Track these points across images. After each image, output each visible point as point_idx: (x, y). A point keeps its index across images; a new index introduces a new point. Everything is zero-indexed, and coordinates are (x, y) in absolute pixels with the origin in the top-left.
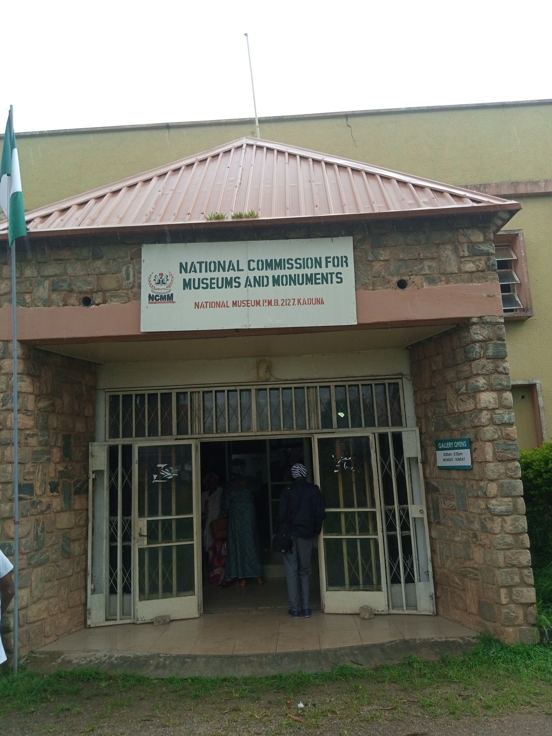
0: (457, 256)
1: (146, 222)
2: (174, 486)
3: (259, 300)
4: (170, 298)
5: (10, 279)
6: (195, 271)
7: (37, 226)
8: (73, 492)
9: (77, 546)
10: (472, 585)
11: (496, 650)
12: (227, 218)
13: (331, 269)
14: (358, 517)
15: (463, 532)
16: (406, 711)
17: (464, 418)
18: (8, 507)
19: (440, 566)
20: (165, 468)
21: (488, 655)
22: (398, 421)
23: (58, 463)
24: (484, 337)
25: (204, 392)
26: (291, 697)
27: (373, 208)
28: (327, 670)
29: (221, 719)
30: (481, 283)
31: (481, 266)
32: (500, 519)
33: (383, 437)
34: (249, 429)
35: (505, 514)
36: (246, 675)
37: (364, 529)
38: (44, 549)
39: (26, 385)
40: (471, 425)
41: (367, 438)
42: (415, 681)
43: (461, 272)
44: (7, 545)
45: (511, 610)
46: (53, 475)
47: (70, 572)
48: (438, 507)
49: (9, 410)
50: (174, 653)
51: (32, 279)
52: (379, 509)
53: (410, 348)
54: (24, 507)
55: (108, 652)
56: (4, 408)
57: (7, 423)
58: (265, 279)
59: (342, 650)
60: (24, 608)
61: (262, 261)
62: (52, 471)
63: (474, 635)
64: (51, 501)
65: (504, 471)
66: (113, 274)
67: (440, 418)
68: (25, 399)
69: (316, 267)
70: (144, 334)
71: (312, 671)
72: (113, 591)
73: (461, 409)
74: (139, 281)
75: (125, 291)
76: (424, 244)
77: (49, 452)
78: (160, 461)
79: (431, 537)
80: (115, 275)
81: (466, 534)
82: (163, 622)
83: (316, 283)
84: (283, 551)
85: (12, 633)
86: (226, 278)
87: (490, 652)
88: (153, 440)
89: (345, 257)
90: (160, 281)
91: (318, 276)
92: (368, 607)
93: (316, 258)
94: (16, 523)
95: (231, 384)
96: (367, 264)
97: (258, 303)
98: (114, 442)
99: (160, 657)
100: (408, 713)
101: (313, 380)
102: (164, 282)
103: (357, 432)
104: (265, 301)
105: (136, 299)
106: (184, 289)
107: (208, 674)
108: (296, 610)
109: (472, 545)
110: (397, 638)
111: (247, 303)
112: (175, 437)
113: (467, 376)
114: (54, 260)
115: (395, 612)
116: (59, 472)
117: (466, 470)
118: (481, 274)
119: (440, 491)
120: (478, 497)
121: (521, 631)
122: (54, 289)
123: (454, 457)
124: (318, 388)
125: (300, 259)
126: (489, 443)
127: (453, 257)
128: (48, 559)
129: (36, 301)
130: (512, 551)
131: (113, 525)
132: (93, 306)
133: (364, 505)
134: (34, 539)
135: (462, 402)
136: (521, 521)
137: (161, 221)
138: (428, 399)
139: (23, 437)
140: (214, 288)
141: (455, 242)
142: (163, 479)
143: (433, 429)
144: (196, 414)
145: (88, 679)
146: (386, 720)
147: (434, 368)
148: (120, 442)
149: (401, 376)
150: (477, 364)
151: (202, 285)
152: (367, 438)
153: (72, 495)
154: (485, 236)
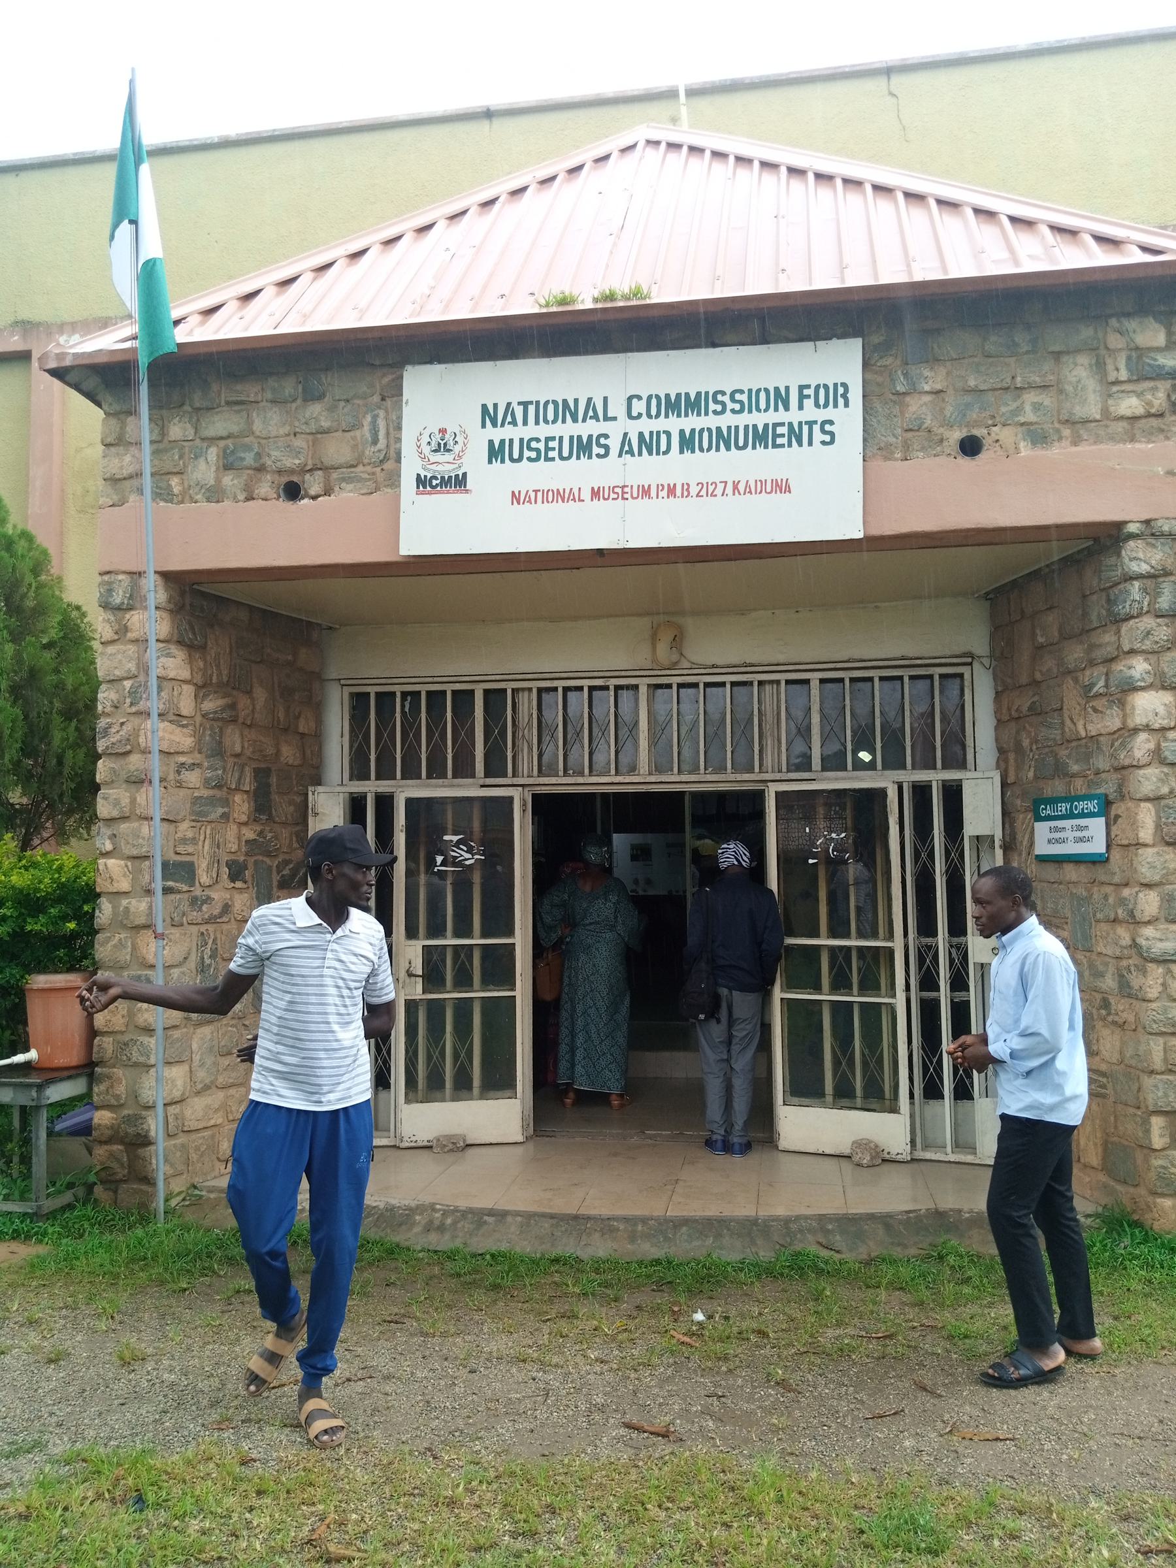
0: (1101, 381)
2: (477, 878)
4: (460, 482)
5: (138, 444)
6: (514, 423)
8: (275, 883)
11: (1132, 1240)
12: (583, 301)
13: (811, 412)
14: (859, 958)
17: (1098, 748)
20: (459, 842)
21: (1113, 1250)
22: (957, 757)
23: (246, 824)
26: (682, 1300)
27: (910, 273)
28: (765, 1254)
29: (536, 1330)
30: (1153, 442)
31: (1156, 403)
32: (1160, 970)
33: (921, 792)
34: (633, 769)
36: (601, 1253)
39: (176, 664)
41: (882, 793)
43: (1108, 419)
44: (143, 978)
50: (463, 1204)
51: (185, 444)
53: (991, 596)
56: (134, 709)
58: (663, 438)
61: (658, 397)
62: (233, 838)
64: (231, 899)
67: (1047, 750)
68: (175, 693)
69: (776, 409)
70: (412, 560)
71: (734, 1257)
73: (1093, 730)
75: (369, 468)
76: (1027, 352)
77: (226, 802)
78: (450, 831)
80: (348, 435)
82: (451, 1146)
83: (775, 446)
84: (702, 1017)
85: (152, 1148)
86: (580, 437)
88: (437, 786)
89: (844, 385)
91: (780, 430)
92: (871, 1142)
93: (777, 389)
96: (892, 401)
97: (645, 492)
98: (358, 787)
99: (434, 1210)
100: (916, 1347)
101: (775, 667)
102: (448, 447)
104: (660, 488)
106: (490, 462)
107: (525, 1247)
108: (719, 1137)
110: (924, 1205)
111: (621, 493)
112: (481, 782)
113: (1109, 656)
114: (228, 403)
115: (929, 1155)
117: (1094, 863)
118: (1154, 422)
122: (227, 466)
123: (1070, 835)
124: (783, 683)
125: (741, 392)
126: (1148, 805)
127: (1091, 384)
129: (191, 492)
132: (306, 501)
133: (875, 935)
135: (1095, 715)
138: (1025, 709)
139: (173, 767)
140: (553, 459)
141: (1097, 348)
142: (454, 864)
143: (1031, 774)
144: (523, 736)
145: (295, 1242)
147: (1041, 640)
148: (371, 787)
149: (969, 658)
150: (1131, 629)
151: (527, 453)
153: (275, 889)
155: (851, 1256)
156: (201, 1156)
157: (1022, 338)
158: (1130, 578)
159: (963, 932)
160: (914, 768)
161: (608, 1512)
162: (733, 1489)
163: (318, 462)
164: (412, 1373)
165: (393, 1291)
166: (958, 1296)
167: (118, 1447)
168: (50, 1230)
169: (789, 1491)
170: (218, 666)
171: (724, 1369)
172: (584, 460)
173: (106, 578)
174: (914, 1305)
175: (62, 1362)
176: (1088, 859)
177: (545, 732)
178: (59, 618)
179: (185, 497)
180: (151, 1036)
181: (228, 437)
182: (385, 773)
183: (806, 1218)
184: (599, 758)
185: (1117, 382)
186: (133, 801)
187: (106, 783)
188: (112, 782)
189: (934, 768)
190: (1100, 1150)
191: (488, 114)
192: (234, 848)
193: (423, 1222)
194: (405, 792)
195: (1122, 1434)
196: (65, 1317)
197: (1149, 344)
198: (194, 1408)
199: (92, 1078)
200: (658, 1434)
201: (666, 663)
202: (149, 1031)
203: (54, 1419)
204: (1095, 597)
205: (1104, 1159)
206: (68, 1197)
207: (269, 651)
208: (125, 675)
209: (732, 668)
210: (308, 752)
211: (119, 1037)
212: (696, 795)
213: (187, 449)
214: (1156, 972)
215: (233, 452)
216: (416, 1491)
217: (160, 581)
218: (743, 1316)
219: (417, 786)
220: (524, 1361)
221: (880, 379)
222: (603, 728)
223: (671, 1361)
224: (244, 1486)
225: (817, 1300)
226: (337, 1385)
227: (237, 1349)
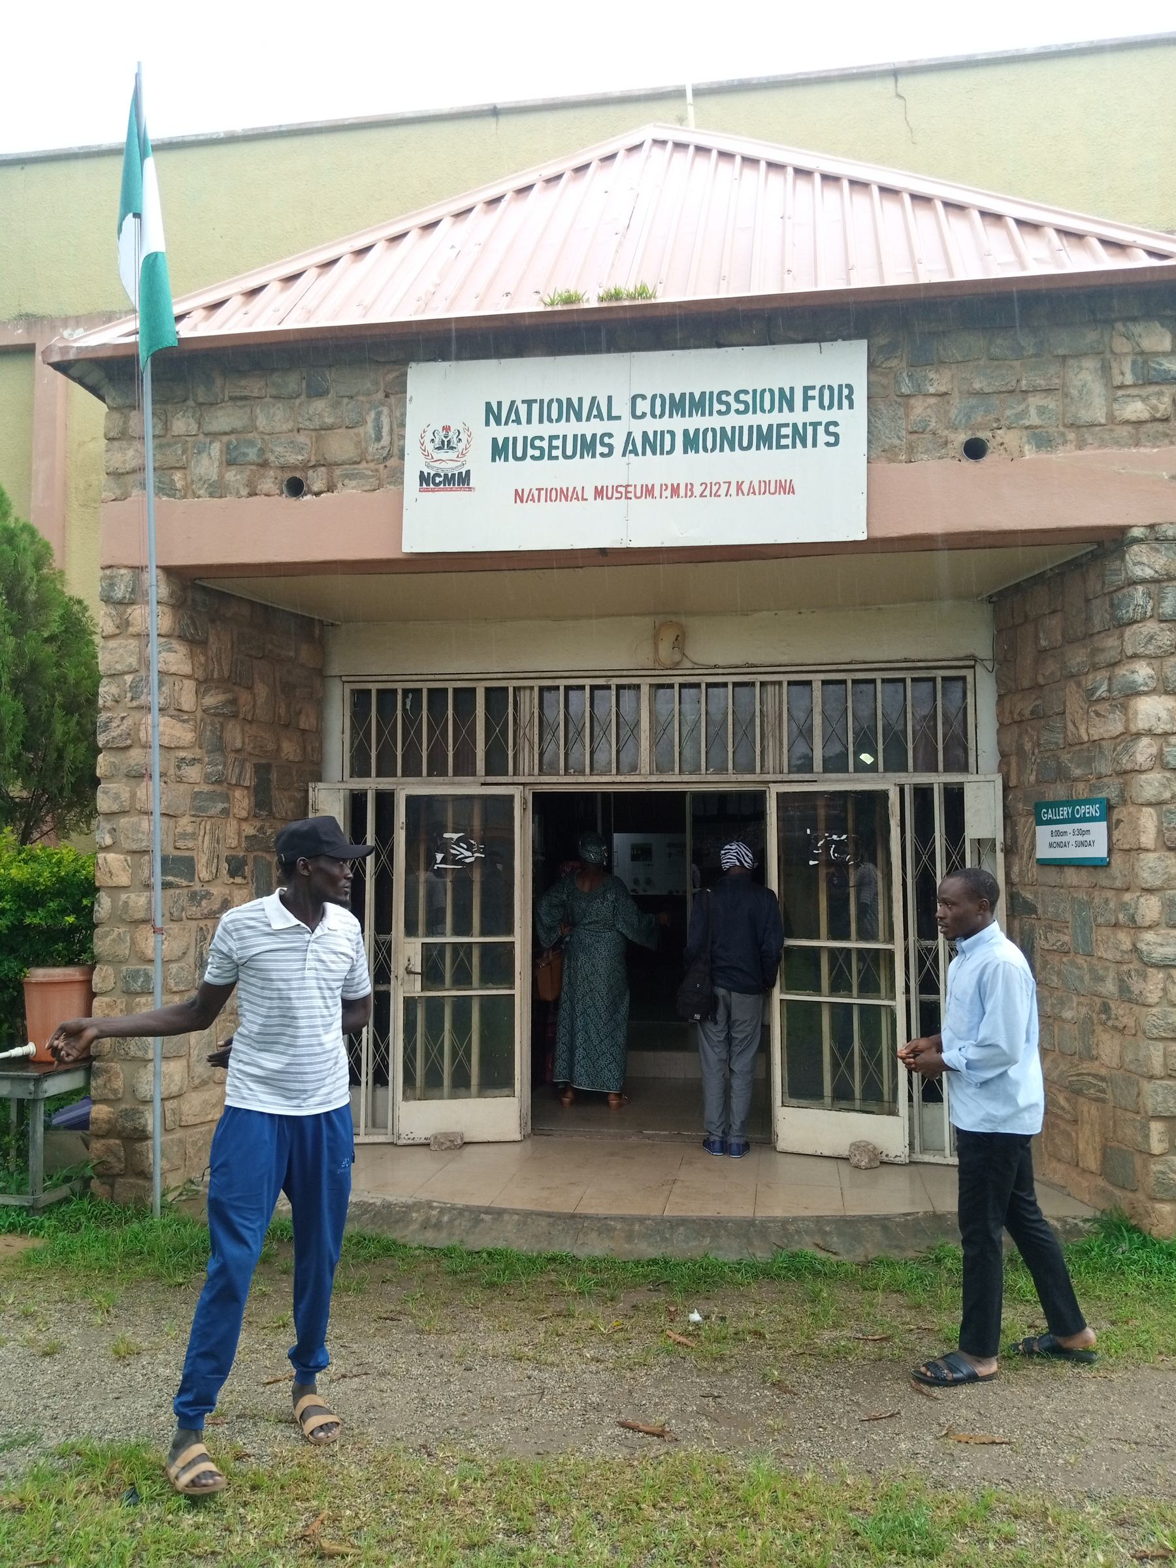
0: (1106, 385)
2: (477, 876)
3: (653, 486)
4: (462, 480)
5: (142, 438)
6: (518, 421)
7: (196, 326)
10: (1094, 1111)
11: (1131, 1246)
12: (588, 300)
13: (815, 413)
15: (1082, 999)
16: (910, 1346)
17: (1100, 752)
18: (142, 900)
20: (459, 840)
22: (959, 760)
23: (245, 820)
24: (1156, 572)
25: (542, 689)
28: (762, 1255)
30: (1158, 447)
31: (1162, 407)
32: (1161, 975)
33: (923, 795)
34: (634, 769)
39: (177, 659)
40: (1114, 770)
41: (884, 795)
42: (942, 1293)
43: (1113, 423)
45: (1170, 1167)
46: (234, 843)
48: (1033, 947)
50: (460, 1202)
51: (188, 439)
53: (994, 599)
56: (135, 704)
58: (668, 437)
59: (799, 1223)
60: (174, 1097)
61: (662, 396)
62: (233, 834)
63: (1088, 1213)
64: (230, 894)
66: (347, 427)
67: (1049, 753)
68: (177, 688)
69: (781, 410)
71: (733, 1258)
73: (1096, 734)
74: (401, 443)
75: (372, 465)
76: (1035, 355)
77: (226, 798)
81: (1087, 1005)
82: (448, 1144)
83: (779, 447)
84: (697, 1017)
85: (150, 1142)
86: (583, 436)
87: (1116, 1250)
89: (849, 387)
90: (443, 442)
91: (784, 431)
92: (869, 1144)
93: (781, 390)
94: (156, 931)
95: (597, 673)
97: (649, 491)
98: (359, 784)
99: (431, 1208)
102: (451, 445)
104: (664, 487)
106: (494, 460)
107: (522, 1245)
108: (717, 1138)
109: (1099, 1029)
110: (922, 1208)
111: (624, 492)
112: (482, 780)
113: (1113, 661)
114: (232, 399)
115: (927, 1158)
116: (246, 837)
117: (1095, 867)
118: (1160, 427)
119: (1039, 912)
120: (1116, 925)
123: (1071, 839)
124: (785, 685)
125: (746, 392)
126: (1150, 810)
127: (1097, 388)
129: (194, 486)
132: (309, 497)
133: (873, 937)
134: (196, 966)
135: (1097, 719)
138: (1027, 713)
139: (173, 762)
140: (557, 458)
143: (1033, 778)
144: (524, 734)
146: (864, 1358)
147: (1044, 643)
148: (371, 784)
149: (972, 661)
150: (1134, 633)
151: (530, 452)
152: (884, 795)
157: (1028, 343)
158: (1133, 583)
159: (388, 930)
160: (915, 770)
162: (727, 1489)
163: (320, 458)
164: (407, 1370)
165: (388, 1288)
167: (112, 1440)
168: (47, 1224)
169: (784, 1493)
170: (219, 661)
171: (720, 1369)
172: (588, 458)
173: (108, 572)
174: (910, 1308)
175: (57, 1356)
176: (1088, 863)
177: (547, 730)
178: (61, 612)
179: (188, 492)
181: (232, 432)
182: (386, 770)
183: (804, 1219)
184: (600, 757)
186: (133, 795)
187: (106, 778)
189: (936, 771)
190: (1099, 1154)
191: (495, 112)
192: (234, 843)
193: (420, 1219)
194: (405, 789)
195: (1118, 1439)
196: (61, 1310)
199: (89, 1072)
200: (654, 1434)
201: (668, 663)
203: (48, 1413)
204: (1098, 602)
205: (1102, 1164)
206: (64, 1191)
207: (270, 647)
208: (126, 669)
210: (309, 748)
213: (190, 445)
215: (235, 447)
216: (411, 1488)
218: (739, 1318)
219: (417, 784)
220: (520, 1359)
221: (884, 381)
222: (605, 727)
223: (667, 1360)
226: (332, 1381)
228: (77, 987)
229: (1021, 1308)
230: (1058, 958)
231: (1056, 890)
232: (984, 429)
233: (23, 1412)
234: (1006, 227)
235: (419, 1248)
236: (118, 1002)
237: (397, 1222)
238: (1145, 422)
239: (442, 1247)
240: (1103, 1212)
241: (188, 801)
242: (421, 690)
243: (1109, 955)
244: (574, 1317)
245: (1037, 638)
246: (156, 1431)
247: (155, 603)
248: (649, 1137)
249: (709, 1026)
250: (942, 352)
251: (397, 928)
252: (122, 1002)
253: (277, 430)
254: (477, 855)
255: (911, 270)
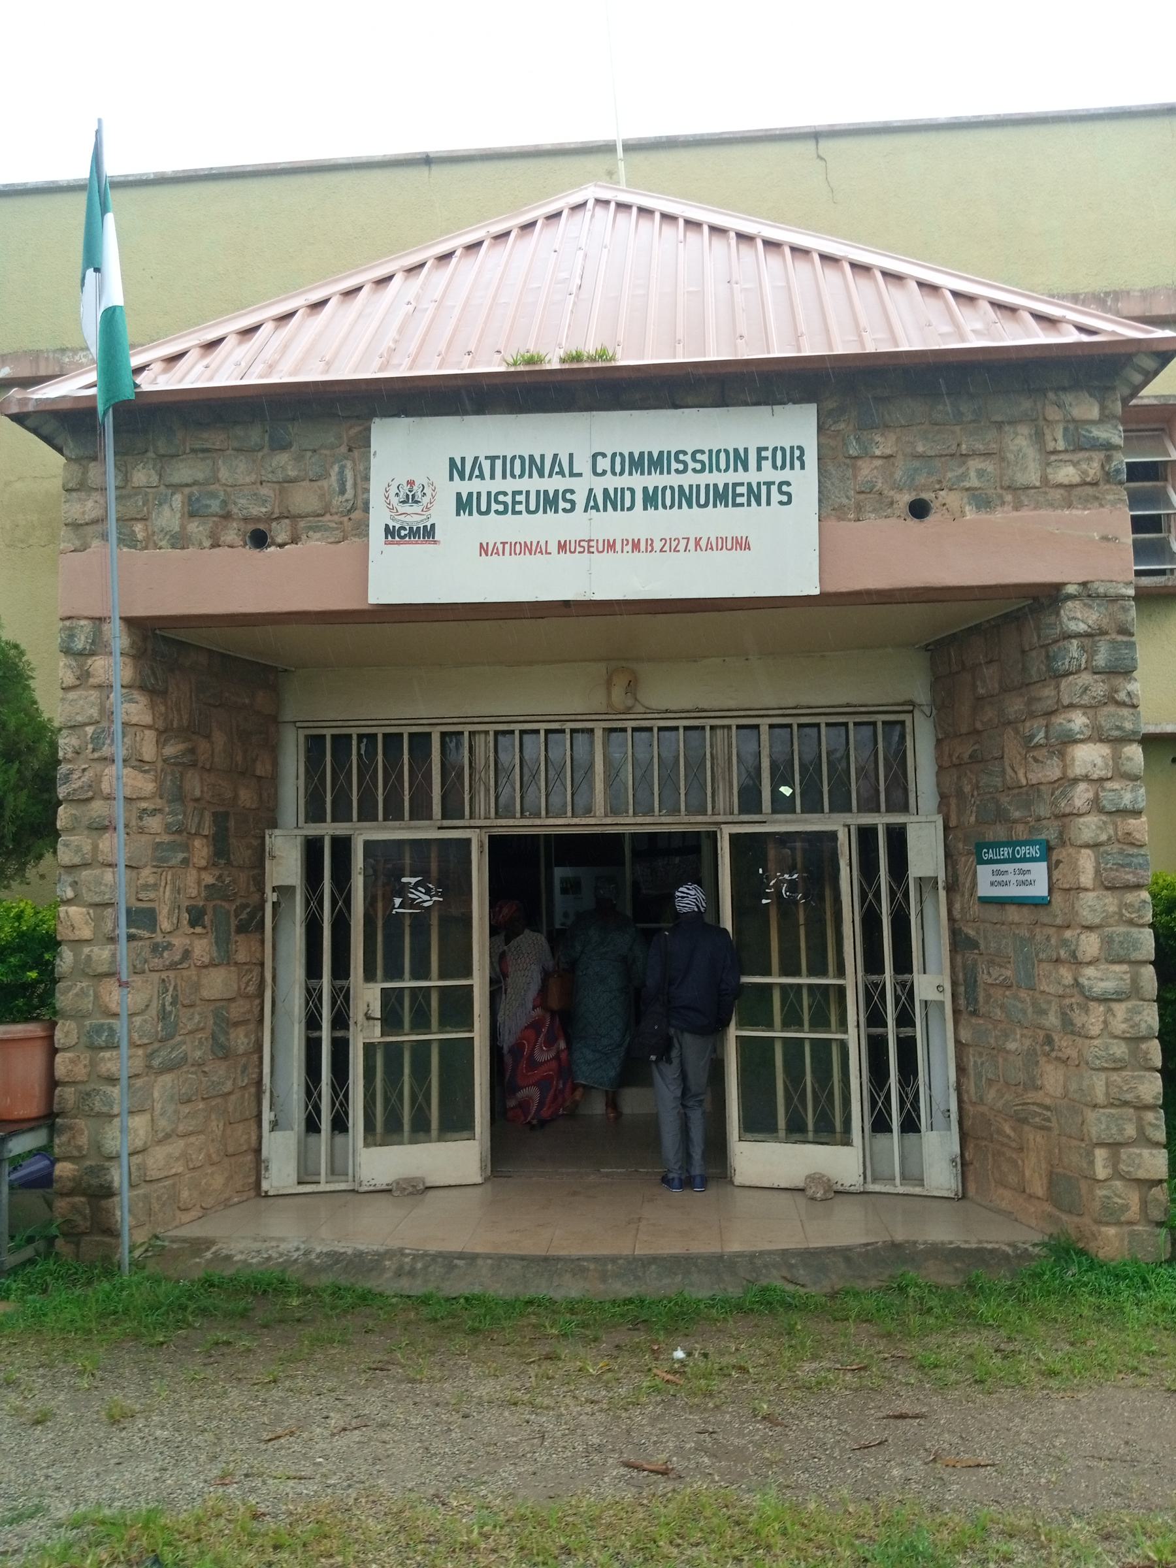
0: (1040, 450)
1: (381, 370)
4: (427, 533)
5: (103, 489)
6: (481, 476)
7: (155, 378)
8: (233, 928)
9: (242, 1036)
10: (1039, 1139)
11: (1080, 1268)
12: (549, 361)
13: (768, 473)
15: (1025, 1031)
16: (887, 1374)
19: (974, 1099)
20: (417, 884)
22: (901, 802)
23: (205, 868)
25: (497, 733)
27: (862, 343)
28: (734, 1292)
31: (1091, 472)
32: (1102, 1008)
33: (867, 835)
34: (589, 811)
35: (1114, 997)
36: (574, 1294)
37: (820, 1021)
38: (178, 1039)
39: (137, 710)
41: (833, 836)
43: (1046, 485)
46: (194, 893)
47: (228, 1086)
48: (976, 981)
49: (105, 759)
50: (433, 1248)
52: (852, 981)
54: (138, 955)
55: (303, 1242)
56: (96, 755)
57: (103, 787)
58: (628, 494)
62: (193, 883)
63: (1037, 1238)
65: (1116, 909)
66: (311, 480)
69: (736, 470)
71: (704, 1294)
72: (312, 1126)
73: (1034, 778)
75: (336, 518)
77: (186, 847)
78: (407, 872)
79: (957, 1042)
82: (411, 1189)
83: (735, 505)
84: (653, 1058)
85: (116, 1199)
86: (546, 492)
89: (800, 448)
90: (407, 496)
91: (739, 490)
93: (736, 451)
97: (611, 546)
98: (314, 830)
101: (726, 712)
103: (812, 823)
105: (358, 535)
106: (458, 514)
107: (498, 1289)
109: (1042, 1060)
110: (880, 1238)
111: (587, 546)
112: (439, 824)
113: (1049, 709)
114: (193, 451)
115: (877, 1188)
117: (1036, 905)
118: (1090, 490)
119: (982, 947)
120: (1058, 960)
121: (1132, 1234)
123: (1013, 878)
124: (734, 728)
125: (703, 452)
126: (1088, 851)
127: (1031, 452)
128: (185, 1059)
130: (1124, 1073)
131: (312, 996)
132: (272, 549)
133: (824, 973)
136: (1145, 1013)
137: (411, 368)
138: (966, 756)
139: (135, 813)
140: (520, 513)
143: (973, 819)
145: (265, 1291)
147: (981, 691)
148: (328, 830)
149: (911, 706)
151: (494, 506)
152: (833, 836)
154: (1103, 408)
155: (816, 1290)
156: (164, 1205)
158: (1069, 636)
159: (347, 976)
160: (859, 811)
161: (622, 1551)
162: (738, 1523)
164: (407, 1421)
165: (373, 1338)
166: (923, 1326)
167: (122, 1507)
168: (14, 1286)
169: (793, 1524)
170: (179, 710)
171: (711, 1405)
173: (67, 623)
174: (882, 1336)
175: (49, 1424)
176: (1029, 901)
177: (502, 775)
179: (148, 543)
180: (114, 1086)
182: (339, 814)
183: (770, 1253)
184: (555, 799)
185: (1055, 452)
188: (74, 828)
189: (878, 811)
190: (1045, 1181)
191: (427, 161)
192: (194, 893)
193: (394, 1267)
194: (362, 834)
195: (1093, 1457)
196: (43, 1376)
197: (1085, 417)
198: (193, 1464)
199: (52, 1130)
200: (657, 1472)
202: (112, 1080)
203: (51, 1483)
204: (1034, 654)
205: (1049, 1188)
206: (28, 1252)
207: (227, 694)
209: (684, 713)
210: (265, 795)
211: (80, 1087)
212: (634, 835)
213: (150, 497)
214: (1099, 1009)
215: (198, 499)
216: (432, 1539)
217: (122, 624)
218: (722, 1354)
220: (515, 1404)
221: (833, 443)
223: (659, 1399)
224: (258, 1542)
225: (789, 1334)
226: (333, 1435)
227: (226, 1402)
228: (39, 1042)
229: (985, 1333)
230: (1001, 992)
231: (998, 926)
232: (928, 490)
233: (24, 1484)
234: (943, 297)
235: (395, 1296)
236: (82, 1057)
237: (371, 1270)
238: (1077, 485)
239: (419, 1294)
240: (1051, 1236)
241: (150, 852)
242: (376, 735)
243: (1051, 989)
244: (560, 1359)
245: (974, 687)
246: (165, 1494)
247: (118, 654)
248: (607, 1175)
249: (664, 1066)
250: (887, 417)
251: (356, 974)
252: (85, 1057)
253: (240, 482)
254: (435, 898)
255: (856, 338)
